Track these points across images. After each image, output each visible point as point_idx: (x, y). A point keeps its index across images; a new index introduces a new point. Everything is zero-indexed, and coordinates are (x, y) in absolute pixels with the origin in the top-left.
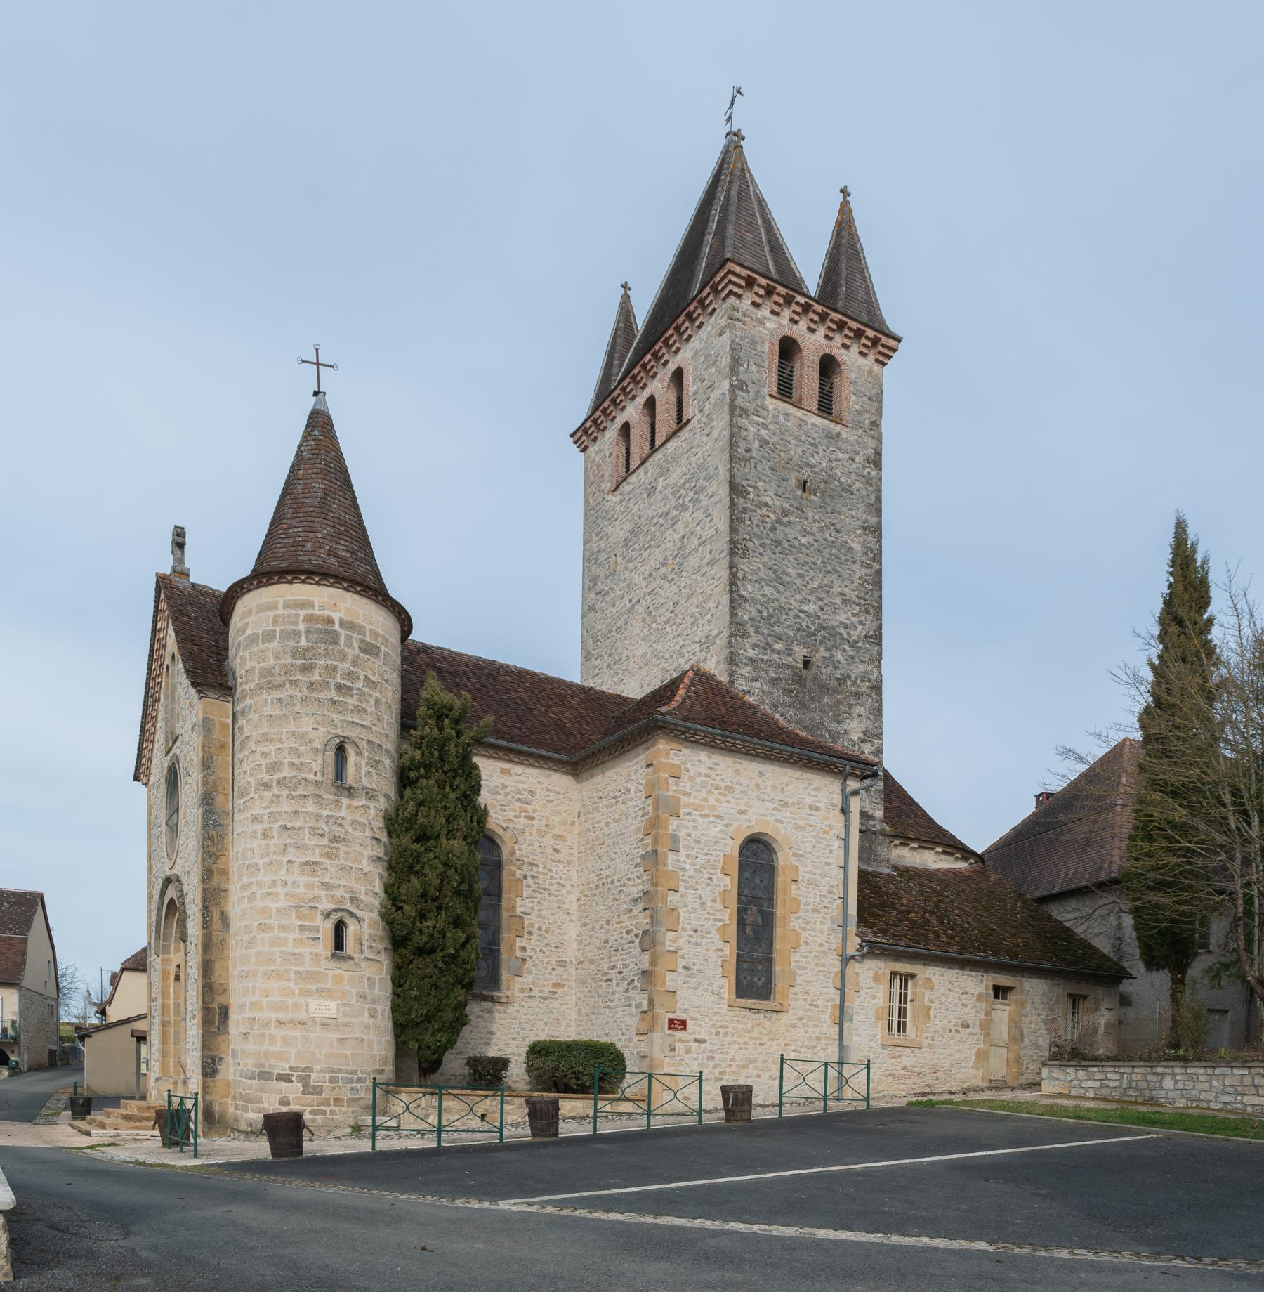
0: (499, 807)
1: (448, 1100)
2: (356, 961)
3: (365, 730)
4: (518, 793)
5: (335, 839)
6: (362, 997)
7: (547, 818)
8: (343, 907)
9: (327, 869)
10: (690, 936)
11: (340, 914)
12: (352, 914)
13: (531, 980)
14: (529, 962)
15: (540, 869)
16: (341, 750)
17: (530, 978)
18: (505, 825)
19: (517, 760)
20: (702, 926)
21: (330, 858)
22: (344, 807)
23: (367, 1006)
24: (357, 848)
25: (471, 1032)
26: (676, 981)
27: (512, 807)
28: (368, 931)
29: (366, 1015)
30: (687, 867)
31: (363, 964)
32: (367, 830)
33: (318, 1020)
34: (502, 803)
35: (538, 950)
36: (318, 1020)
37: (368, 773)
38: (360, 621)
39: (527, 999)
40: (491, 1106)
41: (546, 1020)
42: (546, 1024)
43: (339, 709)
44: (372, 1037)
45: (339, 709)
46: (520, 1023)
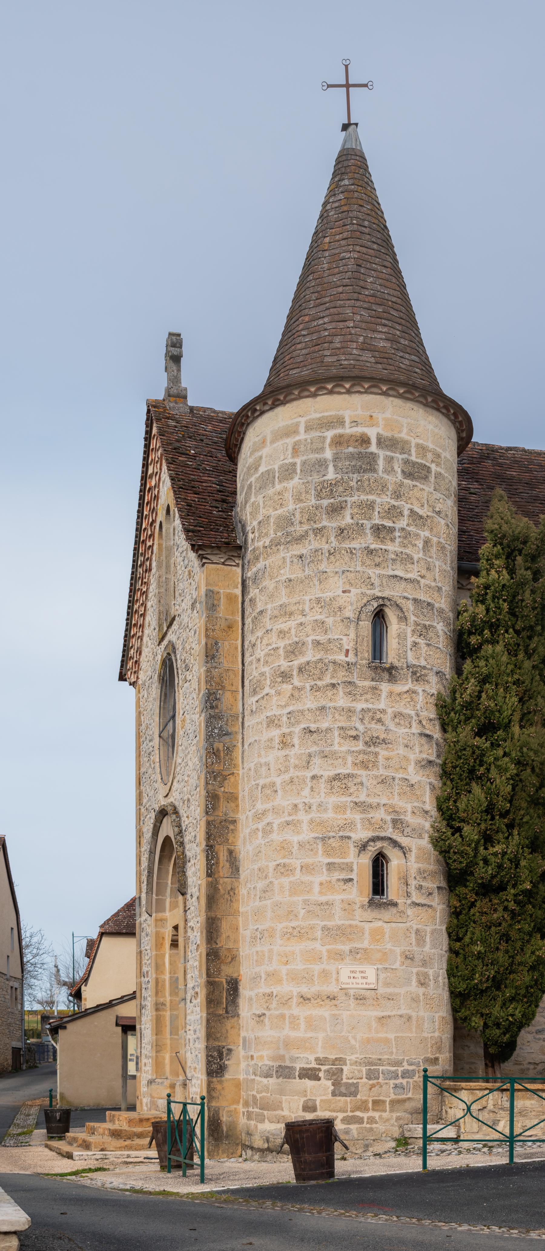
2: (401, 907)
5: (373, 741)
6: (409, 958)
8: (383, 834)
11: (379, 844)
12: (395, 843)
16: (379, 617)
22: (384, 695)
23: (415, 970)
24: (401, 751)
31: (410, 912)
32: (414, 724)
33: (352, 992)
36: (352, 992)
37: (415, 644)
43: (377, 560)
44: (421, 1013)
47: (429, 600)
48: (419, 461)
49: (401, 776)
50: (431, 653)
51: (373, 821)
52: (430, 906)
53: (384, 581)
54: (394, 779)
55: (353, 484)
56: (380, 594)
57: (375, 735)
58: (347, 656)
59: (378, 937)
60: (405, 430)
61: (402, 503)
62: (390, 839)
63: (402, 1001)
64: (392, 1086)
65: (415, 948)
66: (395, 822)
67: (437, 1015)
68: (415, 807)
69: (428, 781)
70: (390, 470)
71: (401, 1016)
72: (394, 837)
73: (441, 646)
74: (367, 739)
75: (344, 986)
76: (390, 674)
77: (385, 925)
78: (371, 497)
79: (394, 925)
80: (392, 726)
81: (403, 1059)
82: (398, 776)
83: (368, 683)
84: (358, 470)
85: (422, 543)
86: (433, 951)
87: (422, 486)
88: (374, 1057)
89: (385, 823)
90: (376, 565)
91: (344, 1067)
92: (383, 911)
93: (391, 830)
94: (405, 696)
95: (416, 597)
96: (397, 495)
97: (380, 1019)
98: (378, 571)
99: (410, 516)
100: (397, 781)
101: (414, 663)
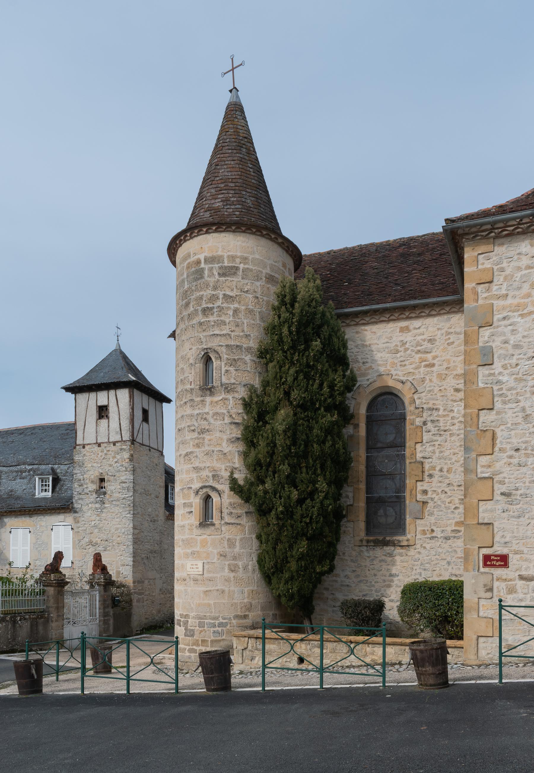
0: (399, 364)
1: (269, 643)
2: (217, 526)
3: (223, 338)
4: (417, 345)
5: (203, 431)
6: (223, 555)
7: (448, 361)
8: (207, 484)
9: (197, 456)
10: (511, 457)
11: (205, 490)
12: (213, 489)
13: (433, 521)
14: (431, 504)
15: (441, 412)
16: (207, 360)
17: (432, 519)
18: (404, 379)
19: (353, 323)
20: (526, 442)
21: (199, 447)
22: (208, 404)
23: (227, 563)
24: (218, 434)
25: (375, 575)
26: (492, 511)
27: (412, 360)
28: (228, 501)
29: (227, 570)
30: (504, 379)
31: (223, 528)
32: (226, 418)
33: (192, 576)
34: (402, 359)
35: (440, 491)
36: (192, 576)
37: (227, 371)
38: (220, 253)
39: (428, 541)
40: (306, 649)
41: (449, 559)
42: (449, 563)
43: (204, 327)
44: (232, 588)
45: (204, 327)
46: (422, 564)
47: (238, 344)
48: (230, 265)
49: (218, 449)
50: (240, 374)
51: (202, 477)
52: (240, 524)
53: (208, 339)
54: (213, 451)
55: (193, 288)
56: (206, 347)
57: (203, 427)
58: (191, 385)
59: (204, 544)
60: (220, 250)
61: (219, 291)
62: (211, 486)
63: (218, 581)
64: (212, 632)
65: (227, 550)
66: (214, 476)
67: (246, 590)
68: (227, 466)
69: (237, 450)
70: (211, 275)
71: (218, 590)
72: (214, 485)
73: (249, 369)
74: (199, 430)
75: (189, 573)
76: (211, 391)
77: (208, 537)
78: (201, 293)
79: (213, 537)
80: (212, 421)
81: (219, 616)
82: (216, 449)
83: (199, 399)
84: (196, 279)
85: (232, 312)
86: (242, 551)
87: (232, 279)
88: (202, 614)
89: (209, 477)
90: (203, 331)
91: (189, 620)
92: (206, 529)
93: (212, 481)
94: (220, 402)
95: (228, 344)
96: (215, 288)
97: (205, 592)
98: (205, 334)
99: (223, 298)
100: (215, 452)
101: (226, 382)
